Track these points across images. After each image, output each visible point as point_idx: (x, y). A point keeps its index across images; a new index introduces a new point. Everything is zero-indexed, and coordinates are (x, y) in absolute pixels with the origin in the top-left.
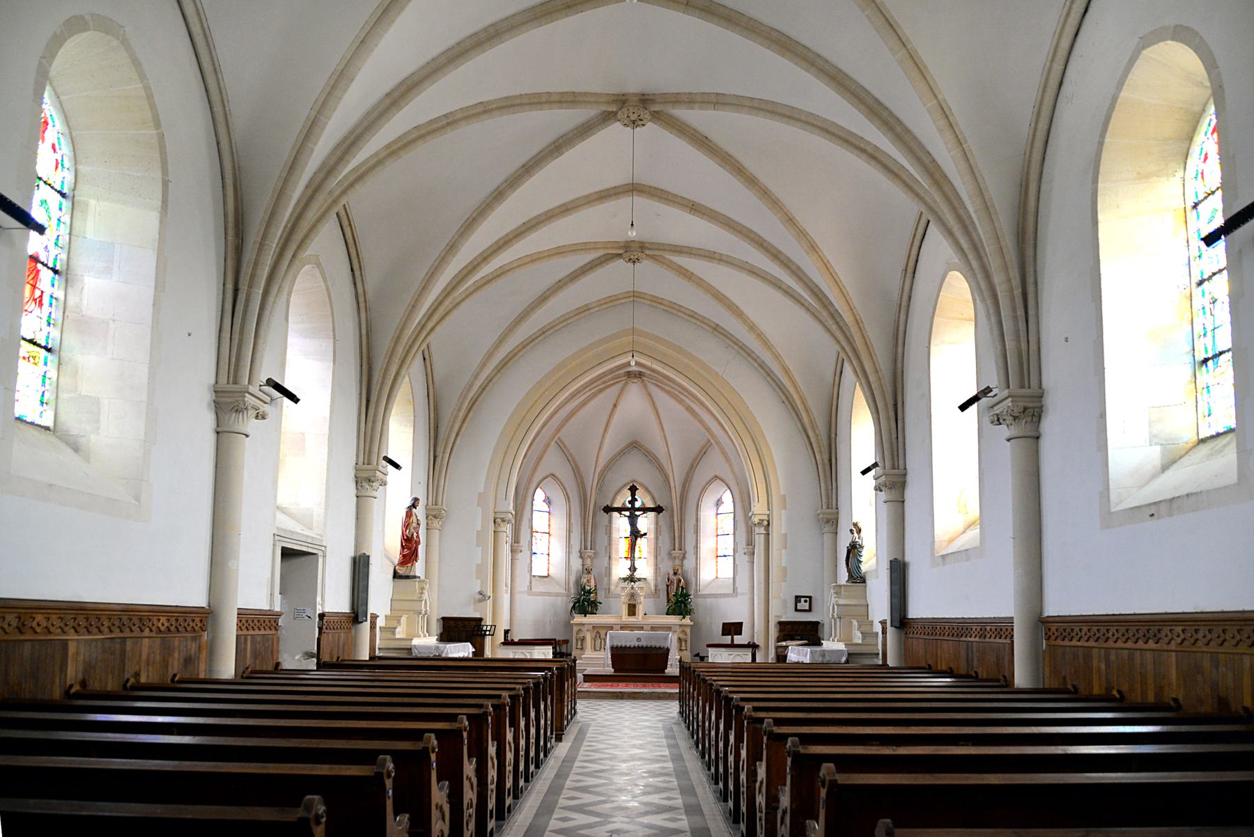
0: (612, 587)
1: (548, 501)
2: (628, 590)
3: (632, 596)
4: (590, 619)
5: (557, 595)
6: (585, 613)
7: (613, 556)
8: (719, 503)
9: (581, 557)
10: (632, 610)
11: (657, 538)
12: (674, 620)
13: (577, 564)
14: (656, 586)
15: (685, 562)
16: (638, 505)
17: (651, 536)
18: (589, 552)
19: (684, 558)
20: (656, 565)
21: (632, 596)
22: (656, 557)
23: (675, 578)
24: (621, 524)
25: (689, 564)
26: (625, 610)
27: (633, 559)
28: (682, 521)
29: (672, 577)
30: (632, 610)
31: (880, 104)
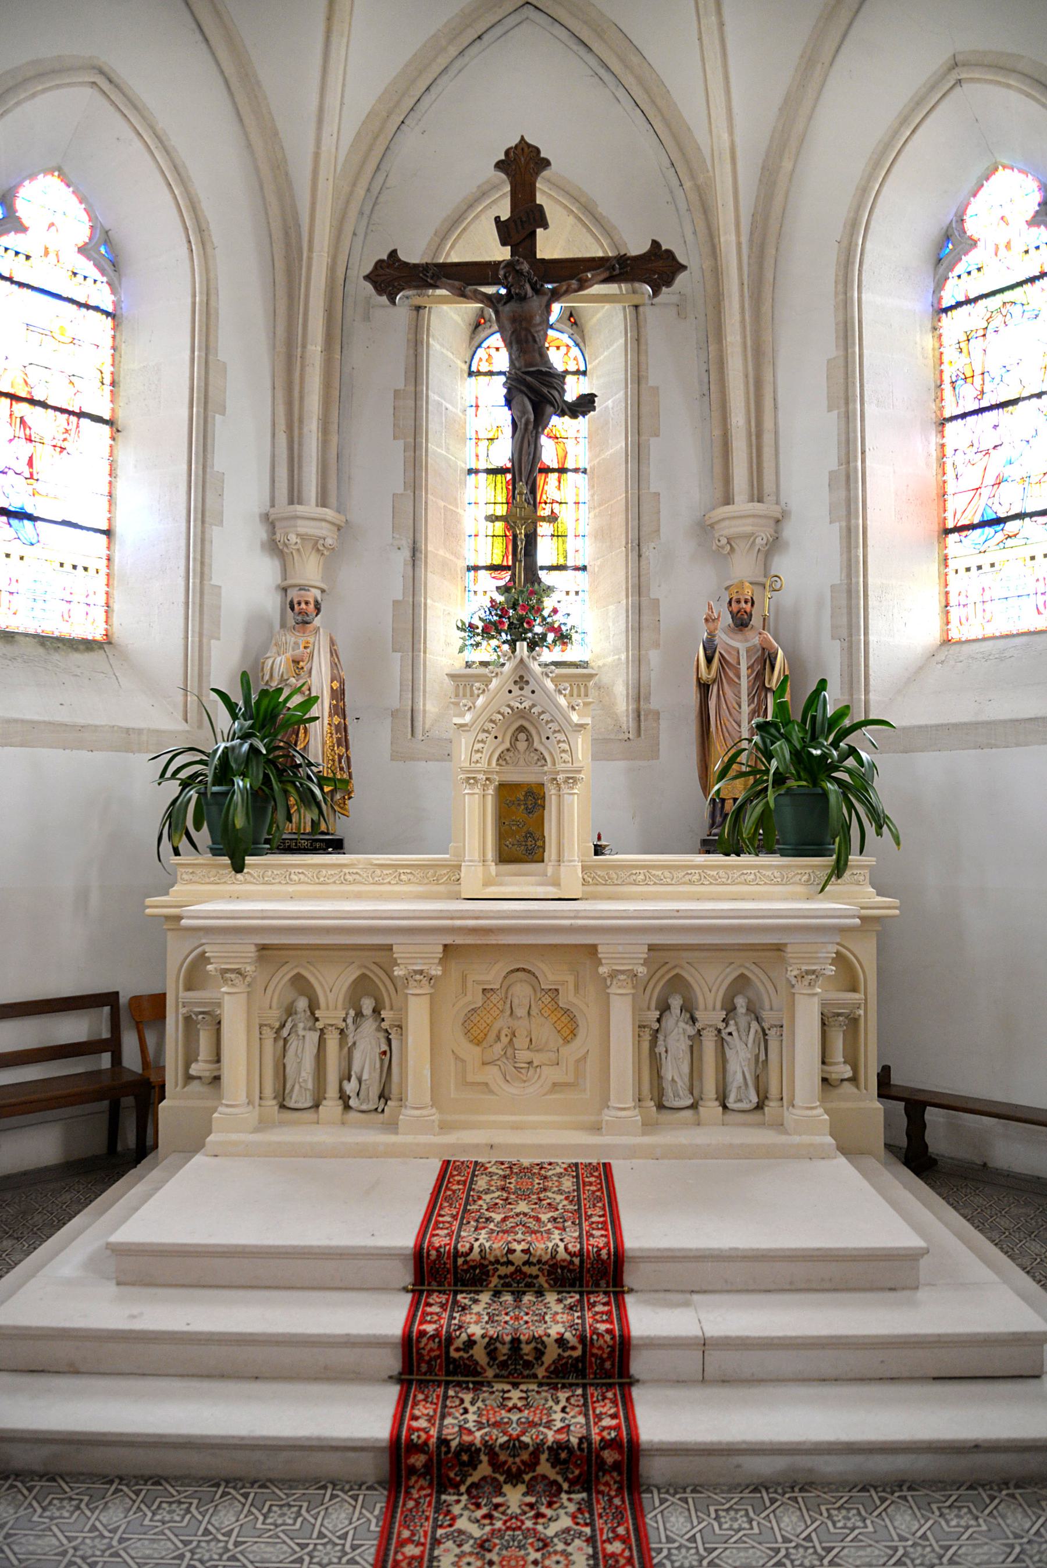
0: (431, 707)
1: (107, 252)
2: (494, 696)
3: (522, 730)
4: (283, 893)
5: (127, 740)
6: (234, 851)
7: (434, 547)
8: (950, 245)
9: (275, 547)
10: (521, 827)
11: (638, 454)
12: (765, 892)
13: (248, 583)
14: (639, 695)
15: (784, 566)
16: (550, 245)
17: (612, 403)
18: (312, 518)
19: (774, 545)
20: (638, 588)
21: (522, 730)
22: (637, 547)
23: (739, 647)
24: (471, 404)
25: (804, 574)
26: (474, 819)
27: (531, 562)
28: (759, 354)
29: (727, 641)
30: (521, 827)
31: (757, 197)
